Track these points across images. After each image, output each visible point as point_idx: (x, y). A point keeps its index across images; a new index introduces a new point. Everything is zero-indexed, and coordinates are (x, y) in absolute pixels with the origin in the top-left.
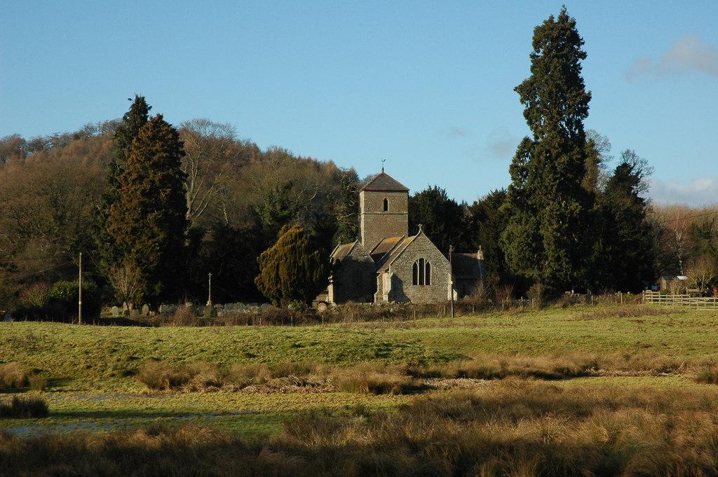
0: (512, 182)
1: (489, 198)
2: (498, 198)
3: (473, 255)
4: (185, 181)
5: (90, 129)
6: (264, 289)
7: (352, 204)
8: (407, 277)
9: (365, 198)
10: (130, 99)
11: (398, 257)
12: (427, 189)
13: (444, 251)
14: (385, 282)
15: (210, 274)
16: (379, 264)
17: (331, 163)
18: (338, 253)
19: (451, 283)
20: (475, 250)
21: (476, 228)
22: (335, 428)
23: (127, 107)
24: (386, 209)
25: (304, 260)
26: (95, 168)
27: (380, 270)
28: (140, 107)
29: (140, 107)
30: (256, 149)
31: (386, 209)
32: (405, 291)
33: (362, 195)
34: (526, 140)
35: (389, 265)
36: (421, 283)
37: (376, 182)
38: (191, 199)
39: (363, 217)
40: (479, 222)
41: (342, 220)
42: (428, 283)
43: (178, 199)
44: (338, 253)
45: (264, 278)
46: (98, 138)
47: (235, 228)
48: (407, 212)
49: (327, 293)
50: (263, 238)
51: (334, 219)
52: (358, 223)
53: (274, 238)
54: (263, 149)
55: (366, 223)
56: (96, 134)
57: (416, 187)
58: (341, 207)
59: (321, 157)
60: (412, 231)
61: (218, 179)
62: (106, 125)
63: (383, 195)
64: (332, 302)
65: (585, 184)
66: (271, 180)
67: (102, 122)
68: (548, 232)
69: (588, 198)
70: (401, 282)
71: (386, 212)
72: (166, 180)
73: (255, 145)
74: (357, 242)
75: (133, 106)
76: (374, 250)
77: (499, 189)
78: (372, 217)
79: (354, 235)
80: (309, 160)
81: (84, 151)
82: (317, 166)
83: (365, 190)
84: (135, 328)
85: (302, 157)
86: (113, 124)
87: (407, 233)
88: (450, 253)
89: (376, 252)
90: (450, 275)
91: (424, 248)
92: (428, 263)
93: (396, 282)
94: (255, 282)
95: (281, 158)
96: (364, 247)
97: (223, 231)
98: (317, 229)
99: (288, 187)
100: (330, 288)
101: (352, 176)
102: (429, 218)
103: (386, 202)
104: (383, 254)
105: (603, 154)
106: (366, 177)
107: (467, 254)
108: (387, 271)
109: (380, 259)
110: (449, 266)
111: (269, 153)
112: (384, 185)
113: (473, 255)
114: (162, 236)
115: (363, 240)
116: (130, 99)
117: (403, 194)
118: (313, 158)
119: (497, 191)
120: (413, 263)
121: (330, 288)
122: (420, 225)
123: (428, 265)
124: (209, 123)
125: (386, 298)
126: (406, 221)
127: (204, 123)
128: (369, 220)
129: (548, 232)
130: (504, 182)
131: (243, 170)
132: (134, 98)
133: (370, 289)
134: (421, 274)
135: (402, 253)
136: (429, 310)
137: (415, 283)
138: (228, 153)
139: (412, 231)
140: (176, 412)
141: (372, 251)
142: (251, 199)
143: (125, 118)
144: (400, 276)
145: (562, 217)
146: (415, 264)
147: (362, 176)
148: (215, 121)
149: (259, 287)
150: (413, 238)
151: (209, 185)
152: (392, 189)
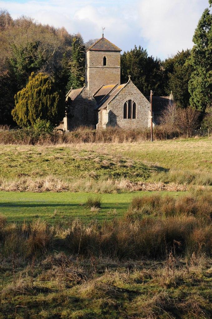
0: (197, 27)
2: (185, 55)
3: (167, 97)
6: (18, 120)
7: (81, 61)
8: (119, 113)
12: (133, 48)
13: (147, 95)
14: (104, 116)
16: (100, 103)
17: (63, 29)
18: (72, 94)
19: (151, 117)
20: (168, 95)
21: (168, 78)
24: (105, 64)
27: (100, 108)
30: (10, 19)
31: (105, 64)
32: (118, 123)
33: (88, 54)
35: (106, 104)
36: (129, 118)
37: (98, 44)
39: (88, 69)
40: (170, 74)
41: (74, 72)
42: (134, 117)
44: (72, 94)
48: (120, 67)
49: (63, 123)
51: (67, 71)
52: (85, 75)
53: (24, 82)
54: (14, 17)
55: (91, 74)
57: (126, 48)
59: (56, 25)
60: (123, 80)
63: (103, 54)
64: (66, 130)
70: (115, 116)
71: (105, 66)
73: (8, 14)
74: (85, 87)
78: (95, 70)
79: (82, 84)
80: (47, 27)
82: (54, 32)
83: (90, 50)
85: (43, 24)
87: (120, 82)
89: (97, 95)
90: (150, 113)
92: (135, 103)
93: (112, 117)
95: (27, 24)
98: (57, 78)
99: (35, 47)
100: (65, 119)
101: (78, 40)
103: (105, 59)
104: (103, 96)
106: (88, 41)
107: (163, 97)
108: (105, 108)
109: (100, 100)
110: (150, 105)
113: (167, 97)
117: (117, 53)
119: (183, 51)
120: (124, 103)
121: (65, 119)
122: (129, 76)
123: (134, 105)
128: (93, 72)
130: (189, 45)
133: (93, 121)
135: (116, 96)
136: (134, 136)
137: (125, 117)
139: (123, 80)
141: (95, 95)
142: (9, 55)
144: (115, 112)
145: (170, 78)
146: (125, 104)
149: (14, 118)
150: (124, 85)
152: (110, 49)
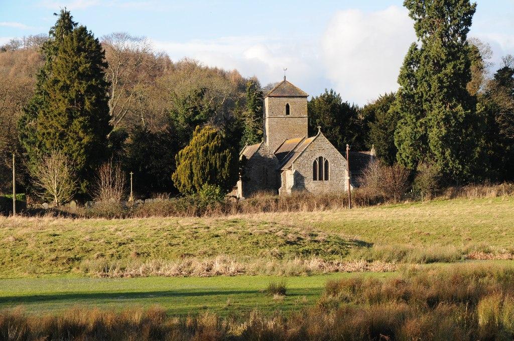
1: (378, 102)
2: (390, 99)
3: (368, 153)
4: (107, 91)
5: (15, 44)
8: (308, 174)
9: (270, 103)
10: (55, 14)
11: (300, 156)
12: (323, 93)
13: (342, 150)
14: (288, 178)
15: (131, 173)
17: (236, 72)
18: (247, 151)
19: (348, 178)
20: (369, 150)
22: (472, 300)
23: (54, 21)
24: (288, 113)
25: (215, 159)
26: (24, 79)
28: (66, 21)
29: (66, 21)
30: (169, 62)
31: (288, 113)
33: (267, 101)
34: (414, 48)
35: (291, 162)
38: (112, 105)
39: (267, 120)
41: (249, 123)
42: (327, 179)
43: (101, 104)
44: (247, 151)
45: (181, 174)
46: (23, 51)
47: (153, 132)
48: (307, 116)
49: (237, 188)
50: (179, 139)
53: (187, 138)
54: (175, 60)
55: (270, 125)
56: (21, 47)
57: (314, 92)
58: (248, 112)
59: (227, 67)
60: (312, 132)
61: (137, 88)
62: (30, 40)
63: (285, 101)
64: (241, 196)
65: (469, 87)
66: (186, 88)
67: (27, 37)
68: (434, 135)
69: (470, 101)
70: (302, 178)
72: (90, 90)
73: (167, 57)
75: (59, 21)
76: (277, 150)
77: (389, 94)
79: (260, 138)
81: (11, 63)
82: (223, 75)
84: (98, 220)
86: (37, 39)
87: (307, 134)
88: (347, 152)
89: (278, 152)
90: (347, 173)
91: (324, 147)
93: (299, 180)
94: (172, 178)
95: (191, 68)
96: (269, 147)
97: (143, 136)
98: (228, 131)
99: (201, 95)
100: (239, 184)
101: (254, 84)
102: (328, 119)
103: (288, 106)
105: (486, 61)
107: (363, 152)
108: (290, 168)
109: (283, 158)
111: (179, 64)
112: (286, 91)
113: (368, 153)
114: (86, 140)
115: (268, 138)
116: (55, 14)
118: (219, 68)
120: (313, 161)
121: (239, 184)
123: (327, 162)
124: (128, 37)
125: (289, 191)
126: (306, 123)
127: (122, 36)
129: (434, 135)
130: (394, 87)
131: (157, 80)
132: (59, 13)
133: (275, 184)
134: (321, 170)
136: (327, 202)
137: (315, 179)
138: (143, 63)
139: (312, 132)
140: (248, 290)
141: (276, 151)
142: (169, 106)
143: (51, 32)
144: (302, 173)
146: (315, 162)
147: (263, 84)
148: (133, 35)
150: (312, 138)
151: (128, 93)
